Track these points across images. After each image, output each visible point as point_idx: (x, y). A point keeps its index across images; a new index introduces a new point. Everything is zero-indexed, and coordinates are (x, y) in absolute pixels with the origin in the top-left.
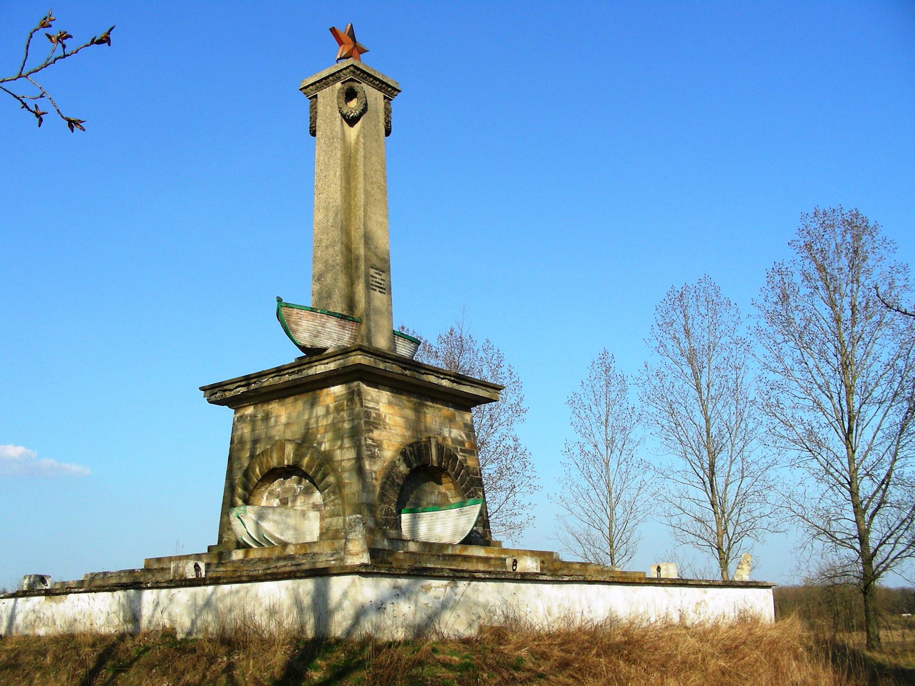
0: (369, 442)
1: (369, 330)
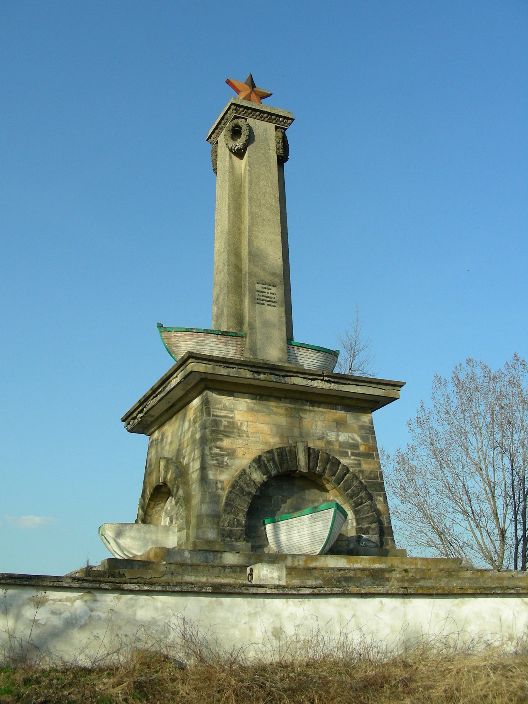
0: (217, 451)
1: (254, 343)
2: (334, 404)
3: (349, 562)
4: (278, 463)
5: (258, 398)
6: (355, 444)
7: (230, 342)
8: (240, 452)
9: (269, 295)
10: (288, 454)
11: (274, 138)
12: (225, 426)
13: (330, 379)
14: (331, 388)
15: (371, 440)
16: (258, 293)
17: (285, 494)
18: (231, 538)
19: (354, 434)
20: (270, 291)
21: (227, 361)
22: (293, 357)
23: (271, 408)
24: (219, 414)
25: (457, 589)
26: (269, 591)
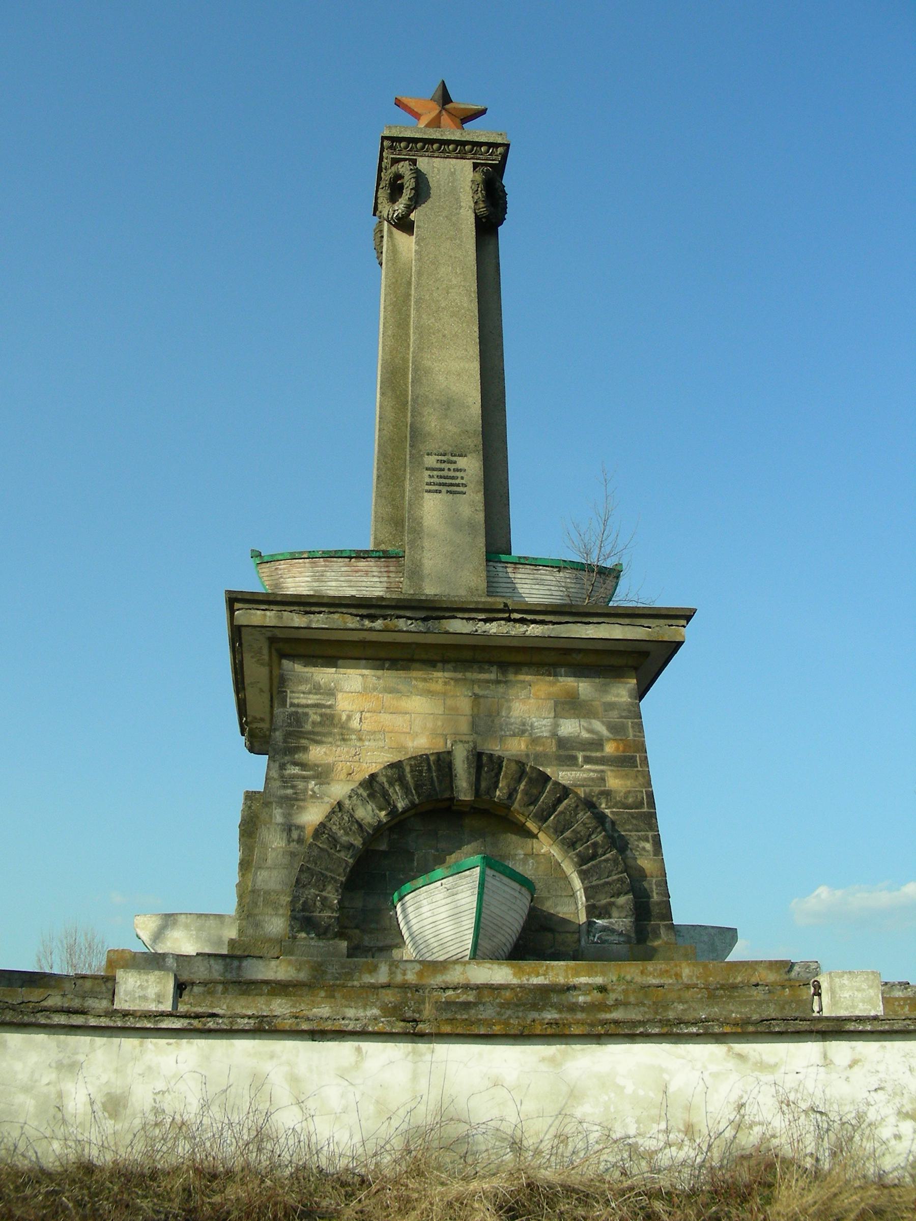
2: (550, 665)
3: (519, 972)
4: (412, 786)
5: (387, 665)
6: (594, 739)
7: (375, 569)
8: (341, 769)
9: (452, 474)
10: (434, 768)
11: (470, 184)
12: (313, 723)
13: (525, 616)
14: (528, 633)
15: (630, 730)
16: (429, 472)
17: (442, 845)
19: (593, 721)
20: (452, 466)
21: (303, 600)
22: (505, 585)
23: (414, 682)
24: (303, 701)
25: (542, 1024)
26: (93, 1022)
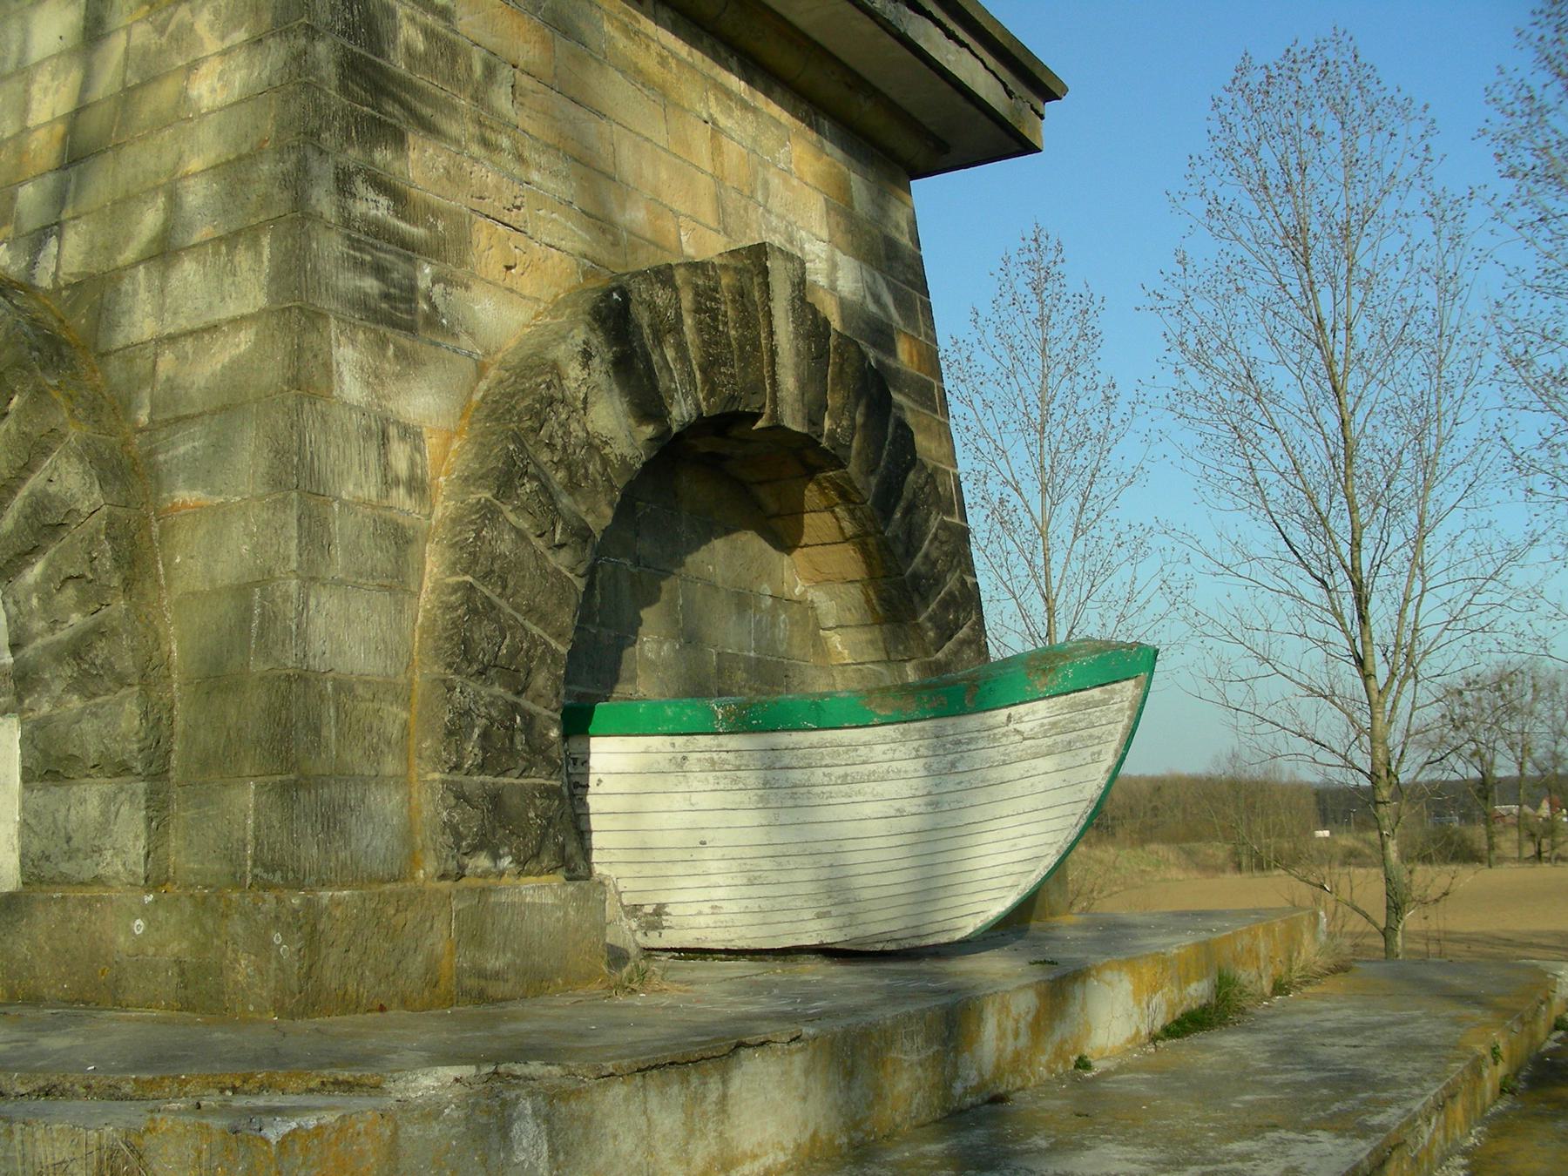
0: (373, 206)
18: (496, 857)
